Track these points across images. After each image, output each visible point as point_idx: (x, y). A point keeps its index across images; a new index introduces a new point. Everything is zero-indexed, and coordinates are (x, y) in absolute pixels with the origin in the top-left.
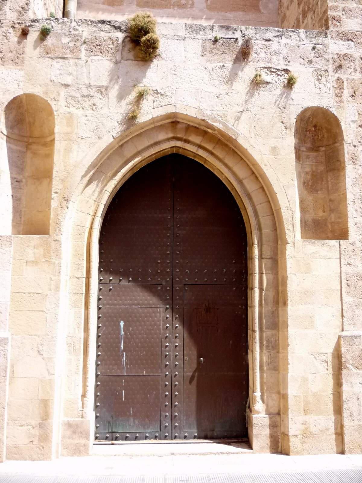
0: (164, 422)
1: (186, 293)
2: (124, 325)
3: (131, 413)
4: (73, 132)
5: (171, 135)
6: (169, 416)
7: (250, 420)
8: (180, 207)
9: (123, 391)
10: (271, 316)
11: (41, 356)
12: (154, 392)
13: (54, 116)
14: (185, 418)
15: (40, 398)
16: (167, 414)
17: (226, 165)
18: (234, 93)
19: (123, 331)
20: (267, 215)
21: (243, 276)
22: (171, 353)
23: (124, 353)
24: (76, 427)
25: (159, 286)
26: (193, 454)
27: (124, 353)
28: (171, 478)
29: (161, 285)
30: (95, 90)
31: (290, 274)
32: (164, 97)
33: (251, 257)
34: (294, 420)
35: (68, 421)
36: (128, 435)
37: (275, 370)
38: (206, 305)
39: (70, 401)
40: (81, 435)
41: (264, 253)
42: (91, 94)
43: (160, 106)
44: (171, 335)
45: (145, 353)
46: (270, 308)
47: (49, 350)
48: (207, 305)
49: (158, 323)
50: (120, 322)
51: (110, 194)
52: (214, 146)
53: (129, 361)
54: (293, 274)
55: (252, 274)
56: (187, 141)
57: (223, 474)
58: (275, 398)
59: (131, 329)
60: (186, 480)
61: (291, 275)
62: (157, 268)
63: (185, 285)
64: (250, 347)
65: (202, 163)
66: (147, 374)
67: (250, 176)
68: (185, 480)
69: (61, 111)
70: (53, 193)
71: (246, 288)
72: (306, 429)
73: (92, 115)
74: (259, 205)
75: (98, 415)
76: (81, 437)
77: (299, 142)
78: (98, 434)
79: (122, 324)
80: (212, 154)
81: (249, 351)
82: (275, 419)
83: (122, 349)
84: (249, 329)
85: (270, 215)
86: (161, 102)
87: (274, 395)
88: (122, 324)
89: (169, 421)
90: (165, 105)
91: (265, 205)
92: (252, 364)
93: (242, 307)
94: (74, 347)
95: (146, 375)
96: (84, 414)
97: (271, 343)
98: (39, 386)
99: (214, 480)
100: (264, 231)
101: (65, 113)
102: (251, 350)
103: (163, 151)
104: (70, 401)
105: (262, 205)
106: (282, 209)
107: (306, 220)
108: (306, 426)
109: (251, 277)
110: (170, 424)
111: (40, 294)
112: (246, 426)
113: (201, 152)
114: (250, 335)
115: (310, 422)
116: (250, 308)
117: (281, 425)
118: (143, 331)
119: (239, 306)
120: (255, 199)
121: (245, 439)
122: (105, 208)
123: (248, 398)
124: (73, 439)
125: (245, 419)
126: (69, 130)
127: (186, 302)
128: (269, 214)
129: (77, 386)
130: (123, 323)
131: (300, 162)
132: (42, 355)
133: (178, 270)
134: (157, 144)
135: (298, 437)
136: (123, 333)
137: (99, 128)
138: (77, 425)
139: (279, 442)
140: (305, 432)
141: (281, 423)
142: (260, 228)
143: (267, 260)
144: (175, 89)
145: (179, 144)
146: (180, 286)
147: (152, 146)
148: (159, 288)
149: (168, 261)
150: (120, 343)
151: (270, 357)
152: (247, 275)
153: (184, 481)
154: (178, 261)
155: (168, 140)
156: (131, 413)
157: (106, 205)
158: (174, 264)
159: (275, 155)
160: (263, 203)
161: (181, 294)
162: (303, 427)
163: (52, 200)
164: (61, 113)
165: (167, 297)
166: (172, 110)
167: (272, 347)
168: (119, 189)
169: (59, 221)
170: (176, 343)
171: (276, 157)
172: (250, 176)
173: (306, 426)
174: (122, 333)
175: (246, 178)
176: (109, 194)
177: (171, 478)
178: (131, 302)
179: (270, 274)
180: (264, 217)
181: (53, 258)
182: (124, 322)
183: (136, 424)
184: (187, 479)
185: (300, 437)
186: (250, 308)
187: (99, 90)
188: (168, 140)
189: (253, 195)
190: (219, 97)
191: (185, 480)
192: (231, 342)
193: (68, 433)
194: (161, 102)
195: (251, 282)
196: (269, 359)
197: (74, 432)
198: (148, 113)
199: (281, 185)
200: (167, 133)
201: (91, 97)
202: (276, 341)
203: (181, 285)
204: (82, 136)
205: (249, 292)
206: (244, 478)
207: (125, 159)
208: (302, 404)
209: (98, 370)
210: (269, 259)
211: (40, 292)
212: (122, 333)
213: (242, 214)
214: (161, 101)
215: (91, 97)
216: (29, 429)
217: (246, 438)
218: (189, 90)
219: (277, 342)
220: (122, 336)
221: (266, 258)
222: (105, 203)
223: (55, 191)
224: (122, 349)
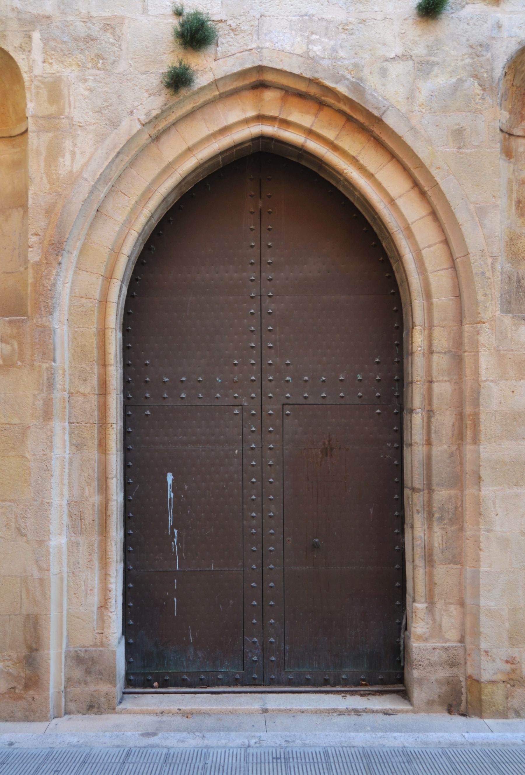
0: (250, 655)
1: (286, 421)
2: (173, 480)
3: (191, 637)
4: (62, 114)
5: (251, 113)
6: (258, 644)
7: (407, 651)
8: (273, 258)
9: (175, 599)
10: (448, 461)
11: (24, 537)
12: (231, 601)
13: (24, 82)
14: (287, 648)
15: (24, 612)
16: (255, 639)
17: (362, 169)
18: (378, 18)
19: (173, 491)
20: (442, 267)
21: (395, 388)
22: (260, 530)
23: (176, 531)
24: (91, 663)
25: (236, 407)
26: (303, 712)
27: (176, 531)
28: (257, 753)
29: (240, 407)
30: (101, 26)
31: (485, 381)
32: (236, 35)
33: (410, 352)
34: (490, 654)
35: (76, 652)
36: (185, 677)
37: (456, 563)
38: (324, 444)
39: (79, 618)
40: (100, 676)
41: (435, 342)
42: (93, 34)
43: (230, 54)
44: (260, 499)
45: (212, 530)
46: (446, 447)
47: (37, 527)
48: (327, 443)
49: (236, 475)
50: (167, 476)
51: (139, 236)
52: (337, 133)
53: (184, 545)
54: (491, 381)
55: (412, 383)
56: (285, 123)
57: (354, 747)
58: (455, 613)
59: (186, 487)
60: (285, 758)
61: (488, 383)
62: (232, 375)
63: (283, 404)
64: (408, 520)
65: (315, 170)
66: (217, 569)
67: (409, 191)
68: (282, 756)
69: (38, 71)
70: (30, 236)
71: (401, 409)
72: (513, 671)
73: (98, 78)
74: (427, 249)
75: (131, 641)
76: (101, 679)
77: (510, 118)
78: (132, 674)
79: (170, 478)
80: (335, 148)
81: (405, 526)
82: (455, 651)
83: (170, 524)
84: (405, 486)
85: (447, 269)
86: (230, 46)
87: (452, 608)
88: (170, 478)
89: (259, 651)
90: (239, 53)
91: (439, 249)
92: (411, 550)
93: (393, 444)
94: (83, 521)
95: (215, 570)
96: (105, 639)
97: (448, 512)
98: (21, 591)
99: (335, 758)
100: (435, 300)
101: (44, 75)
102: (409, 525)
103: (239, 148)
104: (79, 618)
105: (432, 249)
106: (471, 254)
107: (520, 276)
108: (514, 666)
109: (410, 388)
110: (261, 659)
111: (15, 426)
112: (402, 664)
113: (313, 146)
114: (408, 498)
115: (521, 659)
116: (407, 447)
117: (466, 663)
118: (208, 491)
119: (388, 444)
120: (419, 237)
121: (400, 687)
122: (131, 263)
123: (403, 613)
124: (86, 683)
125: (400, 652)
126: (53, 109)
127: (286, 437)
128: (445, 267)
129: (91, 590)
130: (172, 477)
131: (512, 160)
132: (25, 535)
133: (271, 378)
134: (225, 130)
135: (499, 685)
136: (172, 495)
137: (111, 105)
138: (93, 660)
139: (462, 694)
140: (511, 677)
141: (465, 659)
142: (428, 295)
143: (442, 356)
144: (258, 16)
145: (269, 129)
146: (275, 407)
147: (214, 135)
148: (236, 412)
149: (253, 362)
150: (167, 512)
151: (445, 537)
152: (403, 385)
153: (280, 758)
154: (270, 362)
155: (247, 121)
156: (191, 637)
157: (133, 258)
158: (263, 367)
159: (459, 148)
160: (435, 244)
161: (278, 422)
162: (508, 667)
163: (30, 249)
164: (36, 76)
165: (252, 428)
166: (253, 62)
167: (450, 519)
168: (157, 226)
169: (45, 289)
170: (270, 512)
171: (461, 151)
172: (409, 191)
173: (514, 666)
174: (171, 495)
175: (400, 196)
176: (137, 236)
177: (257, 753)
178: (185, 437)
179: (446, 381)
180: (435, 273)
181: (36, 358)
182: (173, 475)
183: (200, 658)
184: (287, 756)
185: (502, 685)
186: (407, 447)
187: (108, 25)
188: (247, 121)
189: (414, 228)
190: (347, 29)
191: (282, 756)
192: (371, 511)
193: (78, 673)
194: (230, 46)
195: (410, 398)
196: (444, 543)
197: (88, 672)
198: (207, 70)
199: (471, 207)
200: (244, 111)
201: (93, 40)
202: (456, 508)
203: (279, 407)
204: (79, 122)
205: (406, 416)
206: (391, 756)
207: (163, 165)
208: (507, 625)
209: (128, 563)
210: (445, 353)
211: (16, 423)
212: (171, 495)
213: (394, 268)
214: (231, 43)
215: (93, 40)
216: (8, 666)
217: (400, 685)
218: (286, 18)
219: (460, 509)
220: (170, 499)
221: (438, 353)
222: (129, 253)
223: (34, 231)
224: (170, 524)
